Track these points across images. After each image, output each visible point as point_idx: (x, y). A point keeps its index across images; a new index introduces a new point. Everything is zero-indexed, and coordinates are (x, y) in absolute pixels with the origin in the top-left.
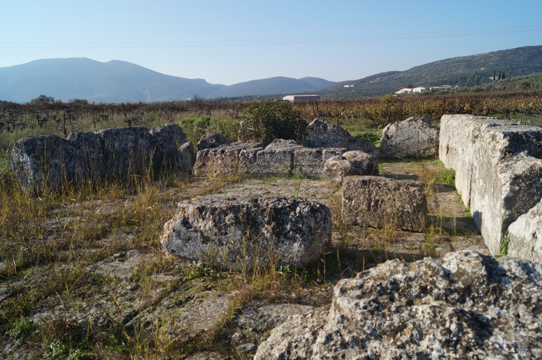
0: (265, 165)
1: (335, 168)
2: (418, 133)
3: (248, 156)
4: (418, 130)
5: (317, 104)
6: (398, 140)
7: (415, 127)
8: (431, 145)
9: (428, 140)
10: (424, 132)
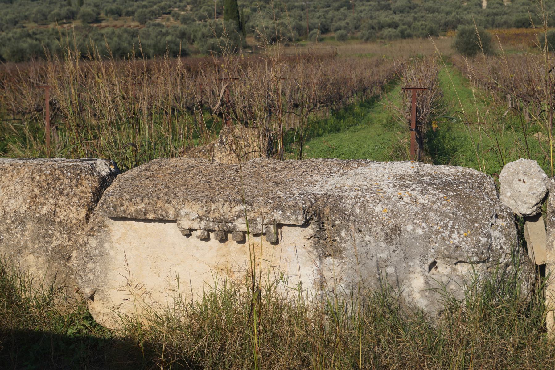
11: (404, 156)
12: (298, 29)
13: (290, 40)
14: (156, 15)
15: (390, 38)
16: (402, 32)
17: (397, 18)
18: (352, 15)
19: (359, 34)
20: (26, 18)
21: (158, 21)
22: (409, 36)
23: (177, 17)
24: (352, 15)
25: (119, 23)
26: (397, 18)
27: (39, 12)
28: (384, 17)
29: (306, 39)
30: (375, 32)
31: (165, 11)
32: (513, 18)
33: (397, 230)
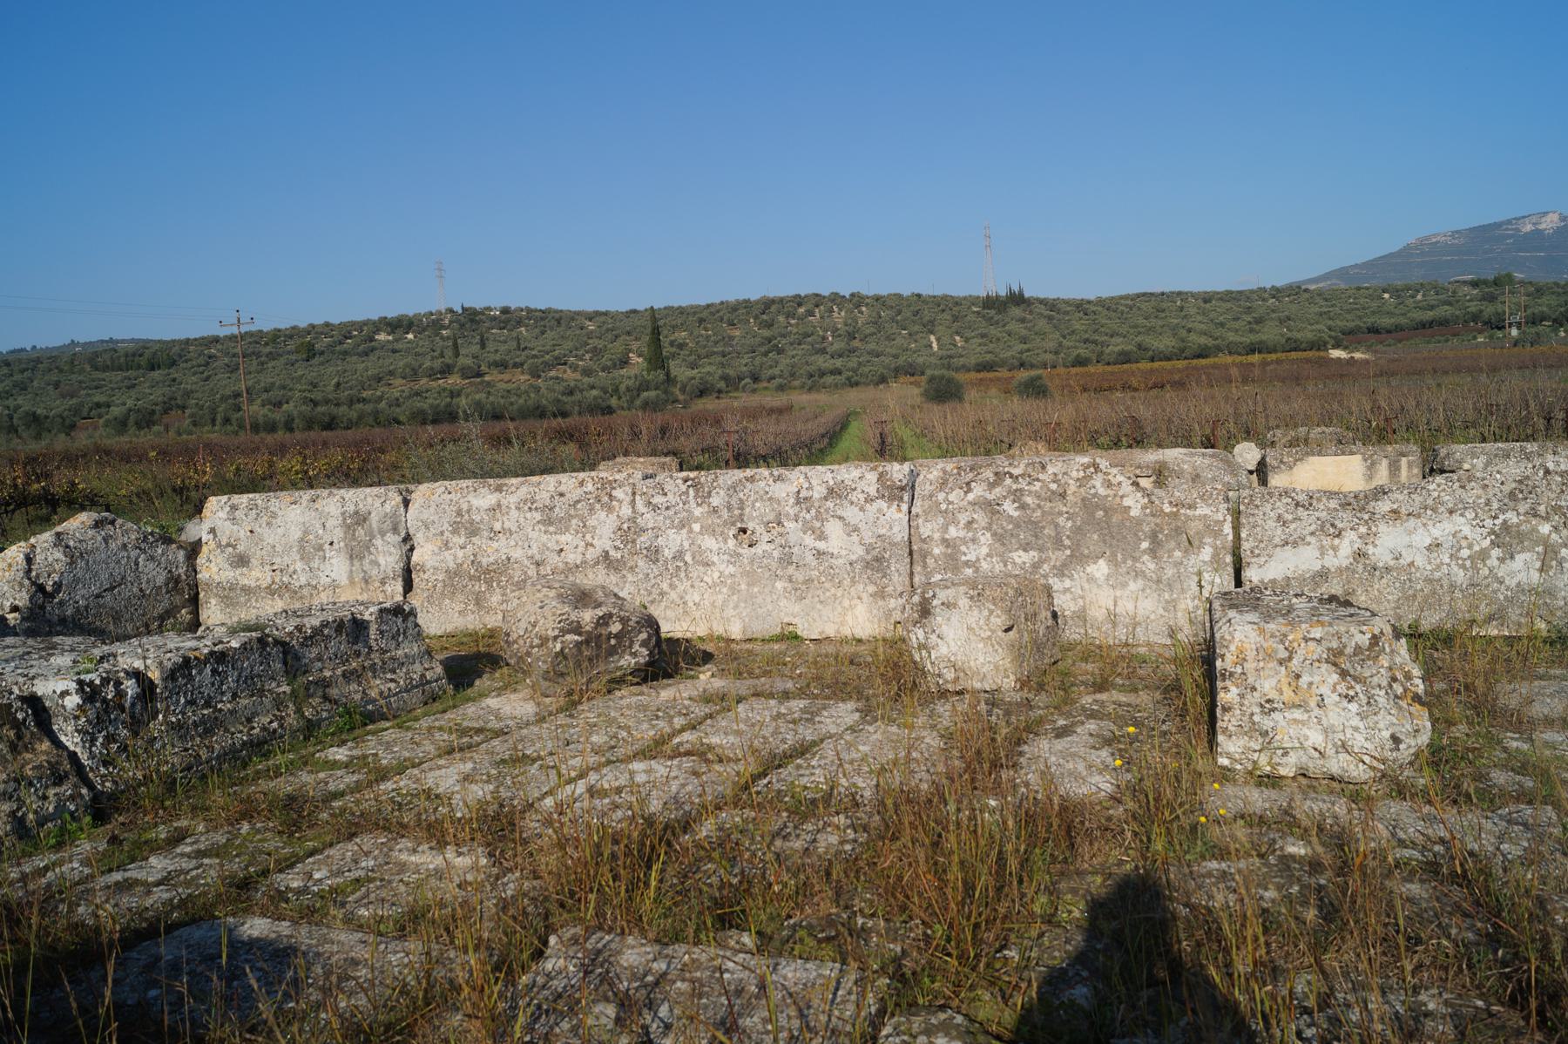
0: (203, 721)
1: (615, 628)
2: (137, 564)
3: (120, 694)
4: (134, 554)
5: (1159, 581)
6: (81, 596)
7: (125, 546)
8: (177, 600)
9: (167, 585)
10: (152, 558)
11: (295, 676)
12: (725, 378)
13: (720, 391)
14: (549, 366)
15: (836, 386)
16: (848, 379)
17: (838, 363)
18: (784, 361)
19: (797, 383)
20: (391, 373)
21: (553, 373)
22: (857, 384)
23: (575, 368)
24: (784, 361)
25: (506, 377)
26: (838, 363)
27: (407, 365)
28: (822, 362)
29: (737, 389)
30: (815, 381)
31: (560, 362)
32: (973, 361)
33: (1198, 476)
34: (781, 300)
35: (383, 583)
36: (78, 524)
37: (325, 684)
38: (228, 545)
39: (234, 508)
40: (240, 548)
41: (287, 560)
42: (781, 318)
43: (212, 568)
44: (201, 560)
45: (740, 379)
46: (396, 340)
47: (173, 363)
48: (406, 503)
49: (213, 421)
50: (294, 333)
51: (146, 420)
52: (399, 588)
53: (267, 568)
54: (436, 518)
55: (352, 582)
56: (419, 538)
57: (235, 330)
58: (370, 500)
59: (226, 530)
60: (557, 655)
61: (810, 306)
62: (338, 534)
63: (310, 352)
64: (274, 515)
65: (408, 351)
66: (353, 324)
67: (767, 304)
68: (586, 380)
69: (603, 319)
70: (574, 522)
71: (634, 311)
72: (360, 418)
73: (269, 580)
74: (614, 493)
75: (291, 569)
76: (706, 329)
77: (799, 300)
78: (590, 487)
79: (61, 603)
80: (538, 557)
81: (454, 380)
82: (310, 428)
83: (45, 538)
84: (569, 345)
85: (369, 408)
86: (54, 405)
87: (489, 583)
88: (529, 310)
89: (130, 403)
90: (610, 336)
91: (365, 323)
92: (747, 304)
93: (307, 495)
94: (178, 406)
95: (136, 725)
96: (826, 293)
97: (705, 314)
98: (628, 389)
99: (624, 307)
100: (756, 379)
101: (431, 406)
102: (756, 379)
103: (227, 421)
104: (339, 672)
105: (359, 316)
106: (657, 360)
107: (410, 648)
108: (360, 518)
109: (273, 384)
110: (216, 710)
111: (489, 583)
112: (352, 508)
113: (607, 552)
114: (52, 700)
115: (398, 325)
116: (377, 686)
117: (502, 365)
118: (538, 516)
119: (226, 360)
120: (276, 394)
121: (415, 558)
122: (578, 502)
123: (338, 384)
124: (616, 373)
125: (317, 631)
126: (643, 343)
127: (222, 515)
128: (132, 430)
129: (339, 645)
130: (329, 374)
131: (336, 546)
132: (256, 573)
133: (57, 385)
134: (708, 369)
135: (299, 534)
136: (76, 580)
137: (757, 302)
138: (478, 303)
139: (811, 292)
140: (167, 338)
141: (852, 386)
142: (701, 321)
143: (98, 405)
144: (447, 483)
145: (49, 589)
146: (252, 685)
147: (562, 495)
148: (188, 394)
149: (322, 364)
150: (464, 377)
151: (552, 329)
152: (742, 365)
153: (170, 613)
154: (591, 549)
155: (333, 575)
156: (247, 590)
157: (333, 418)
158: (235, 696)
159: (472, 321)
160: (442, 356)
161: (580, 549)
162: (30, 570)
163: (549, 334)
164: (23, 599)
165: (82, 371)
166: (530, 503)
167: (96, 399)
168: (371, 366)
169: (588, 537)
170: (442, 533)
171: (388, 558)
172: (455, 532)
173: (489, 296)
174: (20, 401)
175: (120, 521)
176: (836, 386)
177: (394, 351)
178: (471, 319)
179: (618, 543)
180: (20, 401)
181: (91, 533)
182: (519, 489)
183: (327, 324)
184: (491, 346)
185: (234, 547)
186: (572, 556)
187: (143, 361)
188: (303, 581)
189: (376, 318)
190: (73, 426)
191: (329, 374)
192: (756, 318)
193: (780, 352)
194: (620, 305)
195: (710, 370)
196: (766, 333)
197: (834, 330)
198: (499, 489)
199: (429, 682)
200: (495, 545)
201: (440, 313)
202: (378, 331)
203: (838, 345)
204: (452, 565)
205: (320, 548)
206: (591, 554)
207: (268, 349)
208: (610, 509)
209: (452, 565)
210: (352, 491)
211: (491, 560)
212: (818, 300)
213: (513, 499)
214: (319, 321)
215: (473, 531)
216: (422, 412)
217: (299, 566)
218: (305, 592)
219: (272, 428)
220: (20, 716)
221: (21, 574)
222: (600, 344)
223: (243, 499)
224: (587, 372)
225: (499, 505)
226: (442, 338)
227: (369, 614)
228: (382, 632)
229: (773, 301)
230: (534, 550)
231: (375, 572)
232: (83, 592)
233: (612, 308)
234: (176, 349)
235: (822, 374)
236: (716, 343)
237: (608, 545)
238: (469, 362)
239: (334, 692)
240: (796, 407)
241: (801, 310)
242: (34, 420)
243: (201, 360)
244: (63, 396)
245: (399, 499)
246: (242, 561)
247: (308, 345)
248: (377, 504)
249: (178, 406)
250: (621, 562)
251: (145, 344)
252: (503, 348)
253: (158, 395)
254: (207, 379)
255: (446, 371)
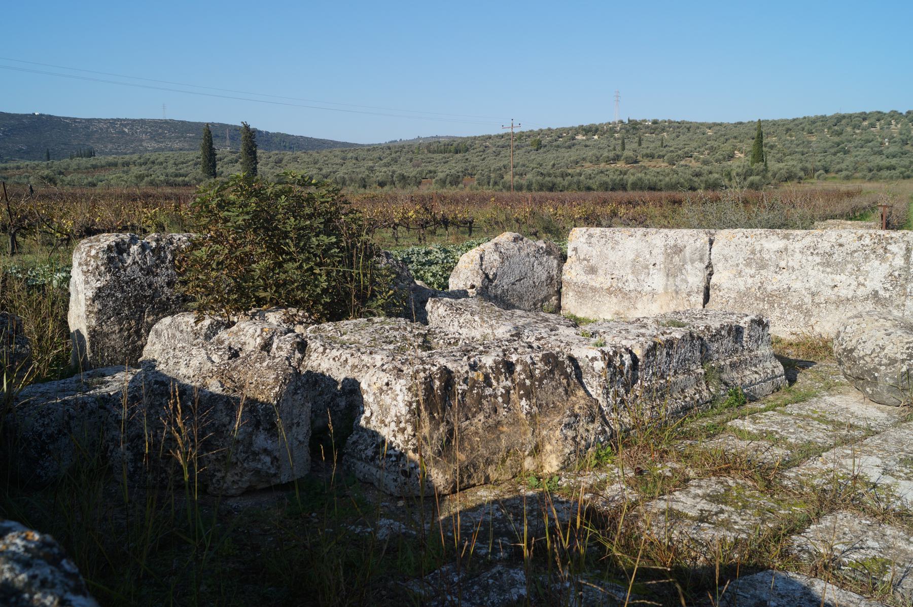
10: (541, 263)
12: (804, 169)
13: (800, 178)
15: (891, 178)
17: (894, 161)
18: (849, 160)
19: (857, 175)
20: (584, 159)
21: (682, 163)
23: (697, 160)
24: (849, 160)
25: (653, 164)
26: (894, 161)
27: (593, 155)
28: (878, 160)
30: (874, 173)
31: (688, 155)
34: (850, 116)
35: (689, 294)
36: (505, 238)
37: (721, 369)
38: (585, 259)
39: (591, 236)
40: (592, 262)
41: (622, 273)
42: (849, 129)
43: (572, 273)
44: (566, 267)
45: (815, 170)
46: (588, 140)
47: (467, 150)
48: (711, 242)
49: (489, 183)
50: (530, 134)
51: (455, 181)
52: (701, 298)
53: (609, 276)
54: (734, 254)
55: (666, 292)
56: (718, 267)
57: (510, 131)
58: (686, 238)
59: (584, 250)
60: (903, 374)
61: (873, 120)
62: (660, 259)
63: (539, 146)
64: (617, 243)
65: (594, 146)
66: (564, 129)
67: (839, 119)
68: (705, 167)
69: (718, 128)
70: (850, 266)
71: (741, 123)
72: (570, 185)
73: (609, 285)
74: (889, 247)
75: (624, 279)
76: (791, 136)
77: (864, 116)
78: (867, 241)
79: (496, 286)
80: (814, 289)
81: (621, 165)
82: (541, 189)
83: (488, 246)
84: (695, 144)
85: (575, 179)
86: (410, 171)
87: (772, 305)
88: (670, 122)
89: (448, 172)
90: (722, 139)
91: (571, 129)
92: (824, 119)
93: (640, 231)
94: (469, 174)
95: (628, 387)
96: (886, 110)
97: (790, 126)
98: (738, 174)
99: (733, 121)
100: (827, 171)
101: (611, 180)
102: (827, 171)
103: (496, 183)
104: (728, 362)
105: (568, 125)
106: (759, 155)
107: (764, 350)
108: (678, 250)
109: (518, 163)
110: (667, 381)
111: (772, 305)
112: (673, 242)
113: (877, 292)
114: (584, 362)
115: (589, 130)
116: (749, 375)
117: (651, 156)
118: (818, 259)
119: (494, 149)
120: (519, 169)
121: (714, 280)
122: (855, 251)
123: (554, 165)
124: (725, 164)
125: (718, 332)
126: (749, 145)
127: (583, 240)
128: (448, 186)
129: (728, 343)
130: (549, 158)
131: (657, 267)
132: (601, 279)
133: (411, 160)
134: (791, 163)
135: (632, 257)
136: (504, 273)
137: (831, 117)
138: (638, 118)
139: (874, 110)
140: (465, 136)
141: (904, 178)
142: (788, 130)
143: (430, 172)
144: (744, 230)
145: (491, 277)
146: (684, 366)
147: (841, 245)
148: (474, 167)
149: (545, 152)
150: (627, 163)
151: (684, 134)
152: (817, 161)
153: (546, 298)
154: (862, 288)
155: (653, 286)
156: (594, 289)
157: (554, 184)
158: (676, 372)
159: (634, 128)
160: (614, 149)
161: (852, 287)
162: (482, 265)
163: (682, 137)
164: (478, 283)
165: (423, 153)
166: (813, 250)
167: (429, 168)
168: (573, 154)
169: (861, 279)
170: (737, 265)
171: (694, 278)
172: (748, 265)
173: (645, 113)
174: (394, 168)
175: (525, 239)
176: (891, 178)
177: (586, 146)
178: (634, 127)
179: (888, 286)
180: (394, 168)
181: (512, 244)
182: (801, 239)
183: (549, 129)
184: (644, 145)
185: (588, 261)
186: (845, 292)
187: (452, 148)
188: (632, 287)
189: (577, 125)
190: (420, 183)
191: (549, 158)
192: (829, 128)
193: (846, 152)
194: (729, 117)
195: (792, 163)
196: (836, 139)
197: (891, 138)
198: (786, 237)
199: (776, 377)
200: (779, 277)
201: (615, 123)
202: (577, 133)
203: (893, 149)
204: (743, 288)
205: (647, 267)
206: (861, 292)
207: (516, 143)
208: (883, 259)
209: (743, 288)
210: (673, 231)
211: (775, 287)
212: (879, 116)
213: (798, 246)
214: (545, 127)
215: (762, 266)
216: (606, 183)
217: (630, 277)
218: (633, 294)
219: (519, 188)
220: (569, 370)
221: (478, 266)
222: (715, 144)
223: (596, 231)
224: (706, 162)
225: (786, 249)
226: (615, 139)
227: (744, 323)
228: (751, 337)
229: (844, 117)
230: (812, 284)
231: (683, 287)
232: (506, 280)
233: (725, 121)
234: (469, 143)
235: (880, 169)
236: (798, 145)
237: (878, 287)
238: (631, 153)
239: (725, 376)
240: (864, 191)
241: (866, 123)
242: (403, 178)
243: (481, 149)
244: (414, 166)
245: (707, 239)
246: (592, 270)
247: (538, 141)
248: (691, 241)
249: (469, 174)
250: (890, 300)
251: (454, 139)
252: (652, 145)
253: (460, 167)
254: (483, 159)
255: (617, 158)
